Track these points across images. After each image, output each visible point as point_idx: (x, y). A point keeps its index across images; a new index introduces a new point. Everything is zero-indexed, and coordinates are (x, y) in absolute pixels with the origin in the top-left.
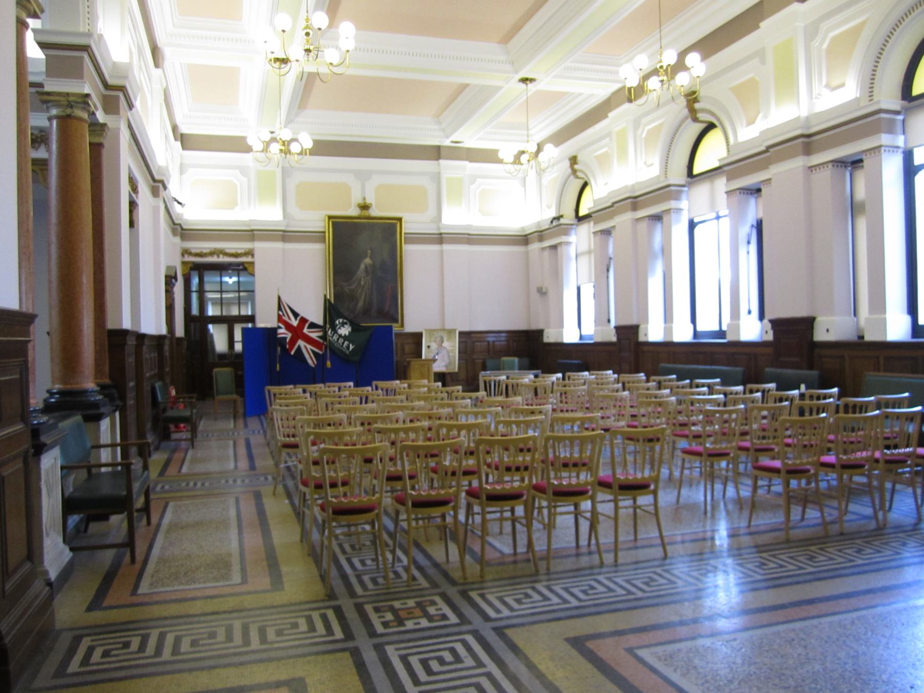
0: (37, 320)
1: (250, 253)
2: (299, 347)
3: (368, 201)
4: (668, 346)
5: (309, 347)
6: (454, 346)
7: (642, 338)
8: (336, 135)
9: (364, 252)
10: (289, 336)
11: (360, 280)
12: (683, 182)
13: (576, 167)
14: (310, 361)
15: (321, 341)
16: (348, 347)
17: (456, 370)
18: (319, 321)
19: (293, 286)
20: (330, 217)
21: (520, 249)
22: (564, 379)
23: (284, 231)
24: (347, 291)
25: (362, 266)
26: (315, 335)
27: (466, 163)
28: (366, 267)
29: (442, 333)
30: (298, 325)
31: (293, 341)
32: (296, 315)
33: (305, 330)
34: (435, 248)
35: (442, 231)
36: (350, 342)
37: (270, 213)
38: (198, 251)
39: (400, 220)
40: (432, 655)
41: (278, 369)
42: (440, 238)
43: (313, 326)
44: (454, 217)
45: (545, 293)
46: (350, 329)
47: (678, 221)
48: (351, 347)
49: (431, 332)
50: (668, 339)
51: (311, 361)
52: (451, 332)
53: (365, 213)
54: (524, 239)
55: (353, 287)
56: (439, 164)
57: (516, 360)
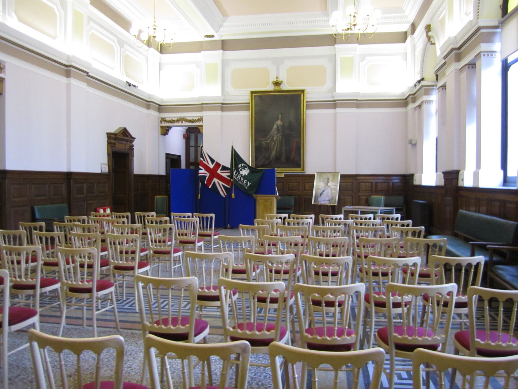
0: (444, 171)
1: (201, 119)
2: (214, 183)
3: (280, 80)
4: (475, 190)
5: (221, 183)
6: (337, 186)
7: (416, 182)
8: (258, 33)
9: (279, 116)
10: (208, 175)
11: (274, 136)
12: (496, 24)
13: (430, 34)
14: (221, 193)
15: (229, 179)
16: (247, 184)
17: (336, 204)
18: (228, 165)
19: (228, 140)
20: (252, 93)
21: (401, 110)
22: (316, 222)
23: (222, 104)
24: (264, 144)
25: (275, 126)
26: (225, 175)
27: (357, 45)
28: (278, 127)
29: (328, 176)
30: (214, 167)
31: (210, 179)
32: (213, 161)
33: (219, 171)
34: (331, 111)
35: (336, 99)
36: (248, 180)
37: (213, 92)
38: (170, 119)
39: (303, 91)
40: (404, 382)
41: (199, 198)
42: (334, 104)
43: (224, 168)
44: (346, 87)
45: (415, 145)
46: (248, 171)
47: (490, 64)
48: (249, 184)
49: (321, 174)
50: (476, 186)
51: (223, 193)
52: (335, 174)
53: (277, 88)
54: (403, 102)
55: (268, 141)
56: (335, 48)
57: (383, 198)
